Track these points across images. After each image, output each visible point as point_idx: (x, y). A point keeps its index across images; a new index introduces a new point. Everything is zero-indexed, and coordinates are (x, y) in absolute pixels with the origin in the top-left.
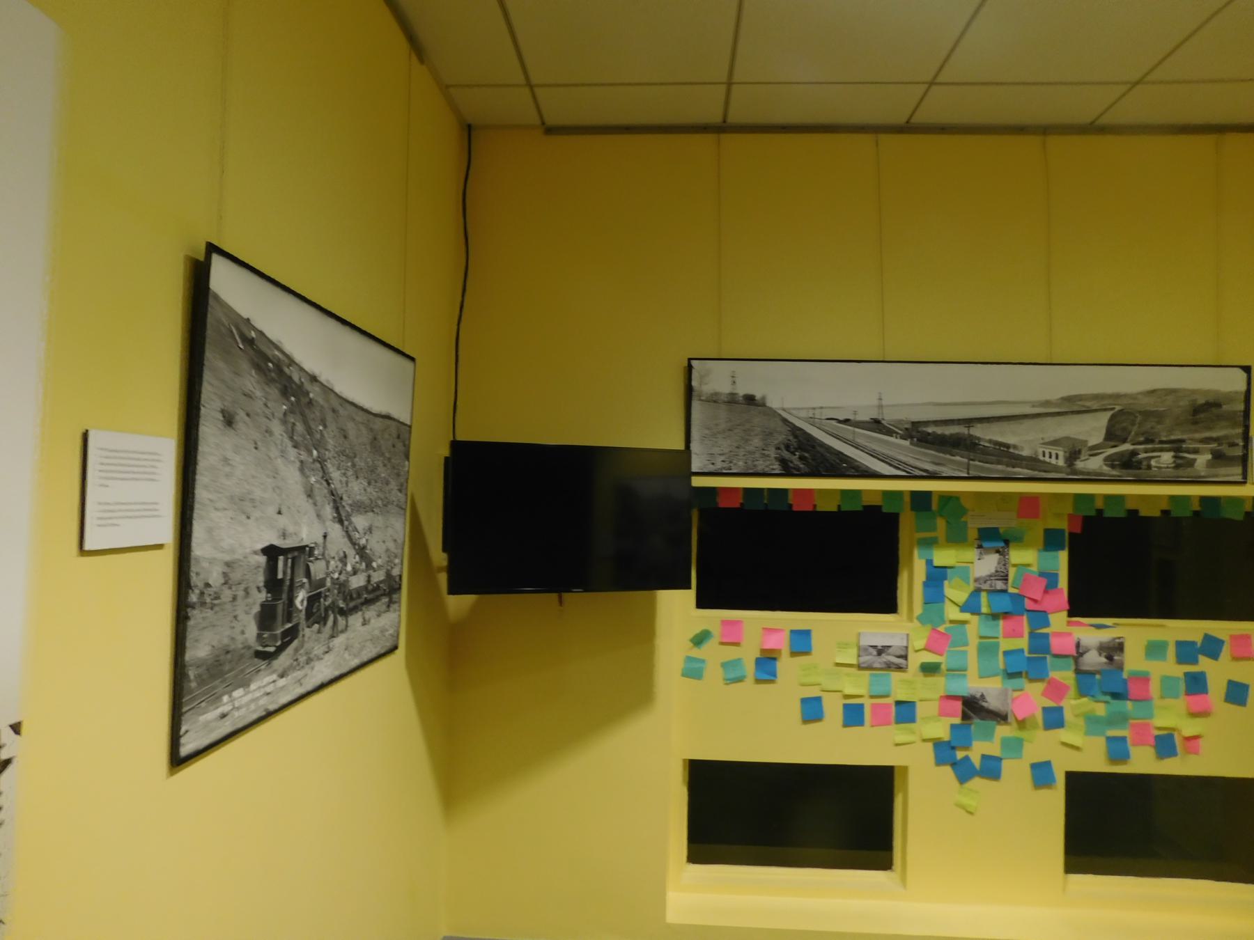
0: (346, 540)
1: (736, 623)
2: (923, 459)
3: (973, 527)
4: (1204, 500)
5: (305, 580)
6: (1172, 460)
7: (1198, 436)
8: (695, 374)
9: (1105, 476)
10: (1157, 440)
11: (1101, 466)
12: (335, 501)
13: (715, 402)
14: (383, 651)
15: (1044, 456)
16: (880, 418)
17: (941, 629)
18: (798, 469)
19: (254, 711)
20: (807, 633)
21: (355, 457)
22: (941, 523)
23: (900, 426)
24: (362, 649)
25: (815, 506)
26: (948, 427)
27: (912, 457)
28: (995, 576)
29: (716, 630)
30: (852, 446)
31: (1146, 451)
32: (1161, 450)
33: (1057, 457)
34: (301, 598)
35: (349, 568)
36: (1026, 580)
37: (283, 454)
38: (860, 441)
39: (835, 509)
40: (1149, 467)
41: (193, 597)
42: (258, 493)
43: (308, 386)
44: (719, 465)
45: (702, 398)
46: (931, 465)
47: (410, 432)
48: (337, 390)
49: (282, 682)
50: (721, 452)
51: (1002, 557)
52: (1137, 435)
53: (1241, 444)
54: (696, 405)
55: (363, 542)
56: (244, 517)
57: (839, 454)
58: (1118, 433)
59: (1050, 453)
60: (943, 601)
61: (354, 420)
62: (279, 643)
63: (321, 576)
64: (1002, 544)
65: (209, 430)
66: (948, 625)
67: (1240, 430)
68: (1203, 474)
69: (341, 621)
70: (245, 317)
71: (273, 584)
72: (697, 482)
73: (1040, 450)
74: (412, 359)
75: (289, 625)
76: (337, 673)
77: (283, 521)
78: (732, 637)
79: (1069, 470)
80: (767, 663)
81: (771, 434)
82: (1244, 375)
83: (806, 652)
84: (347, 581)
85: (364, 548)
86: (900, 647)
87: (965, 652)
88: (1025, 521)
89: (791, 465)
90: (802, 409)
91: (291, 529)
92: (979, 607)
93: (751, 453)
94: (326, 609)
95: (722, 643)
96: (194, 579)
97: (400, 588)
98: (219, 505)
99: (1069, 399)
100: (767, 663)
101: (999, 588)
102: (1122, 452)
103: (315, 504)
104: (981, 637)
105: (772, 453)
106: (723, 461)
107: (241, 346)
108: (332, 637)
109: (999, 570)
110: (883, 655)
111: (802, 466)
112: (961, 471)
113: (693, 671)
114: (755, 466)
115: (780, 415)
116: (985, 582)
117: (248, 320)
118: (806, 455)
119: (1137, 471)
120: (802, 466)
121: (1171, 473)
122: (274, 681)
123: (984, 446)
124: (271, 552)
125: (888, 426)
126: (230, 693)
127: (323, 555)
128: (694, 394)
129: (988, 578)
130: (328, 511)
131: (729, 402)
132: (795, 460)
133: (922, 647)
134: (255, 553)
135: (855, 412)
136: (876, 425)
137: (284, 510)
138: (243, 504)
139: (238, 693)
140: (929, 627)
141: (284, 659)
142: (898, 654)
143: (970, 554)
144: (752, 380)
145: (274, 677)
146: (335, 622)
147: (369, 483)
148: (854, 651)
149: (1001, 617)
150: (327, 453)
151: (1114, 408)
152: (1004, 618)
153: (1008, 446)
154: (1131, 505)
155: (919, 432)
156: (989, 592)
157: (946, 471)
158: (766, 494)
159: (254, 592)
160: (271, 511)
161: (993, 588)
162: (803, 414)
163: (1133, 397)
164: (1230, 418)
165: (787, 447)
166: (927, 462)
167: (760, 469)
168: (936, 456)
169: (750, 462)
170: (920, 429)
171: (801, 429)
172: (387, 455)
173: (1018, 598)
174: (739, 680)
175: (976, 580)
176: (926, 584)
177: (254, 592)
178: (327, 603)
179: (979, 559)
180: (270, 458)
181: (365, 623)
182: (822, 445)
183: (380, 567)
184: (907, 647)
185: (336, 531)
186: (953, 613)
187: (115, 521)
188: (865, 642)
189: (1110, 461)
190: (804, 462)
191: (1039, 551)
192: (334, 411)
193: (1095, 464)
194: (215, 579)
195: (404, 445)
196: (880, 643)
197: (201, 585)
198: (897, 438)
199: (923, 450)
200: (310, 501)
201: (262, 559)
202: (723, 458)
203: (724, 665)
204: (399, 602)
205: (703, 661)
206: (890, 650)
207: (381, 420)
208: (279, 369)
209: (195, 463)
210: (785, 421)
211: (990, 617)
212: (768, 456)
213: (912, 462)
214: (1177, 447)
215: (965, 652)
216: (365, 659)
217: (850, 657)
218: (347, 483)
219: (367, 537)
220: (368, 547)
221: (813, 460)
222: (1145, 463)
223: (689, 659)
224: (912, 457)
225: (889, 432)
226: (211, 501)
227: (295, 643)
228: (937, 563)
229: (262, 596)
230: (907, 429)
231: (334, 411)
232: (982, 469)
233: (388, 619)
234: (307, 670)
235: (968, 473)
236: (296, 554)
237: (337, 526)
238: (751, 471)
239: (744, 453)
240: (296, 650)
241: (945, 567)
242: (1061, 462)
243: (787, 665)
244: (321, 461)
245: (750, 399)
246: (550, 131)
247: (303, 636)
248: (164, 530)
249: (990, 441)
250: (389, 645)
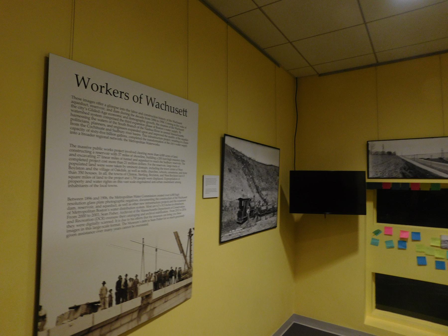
0: (260, 197)
1: (391, 228)
5: (249, 207)
8: (369, 146)
12: (257, 188)
14: (272, 227)
18: (409, 176)
19: (237, 235)
20: (418, 234)
21: (262, 177)
24: (265, 226)
25: (420, 188)
29: (383, 230)
34: (248, 211)
35: (261, 204)
37: (243, 177)
38: (433, 165)
41: (223, 209)
42: (237, 186)
43: (248, 161)
44: (379, 175)
47: (279, 168)
48: (256, 160)
49: (243, 230)
54: (370, 157)
55: (265, 198)
56: (234, 192)
61: (261, 167)
62: (243, 221)
63: (253, 206)
65: (226, 174)
69: (259, 218)
70: (179, 236)
71: (241, 207)
72: (368, 181)
74: (279, 149)
75: (245, 217)
76: (258, 230)
77: (243, 193)
78: (389, 233)
80: (403, 243)
81: (397, 164)
83: (418, 240)
84: (260, 208)
85: (265, 199)
90: (410, 155)
91: (245, 194)
93: (390, 171)
94: (255, 214)
95: (386, 235)
96: (223, 205)
97: (277, 211)
98: (229, 189)
100: (403, 243)
103: (251, 188)
105: (398, 170)
107: (232, 154)
108: (257, 221)
111: (410, 175)
113: (375, 243)
115: (401, 158)
117: (233, 148)
122: (242, 230)
124: (240, 200)
126: (231, 230)
127: (254, 201)
130: (255, 190)
132: (407, 173)
134: (237, 200)
135: (431, 156)
137: (243, 190)
138: (233, 189)
139: (233, 231)
141: (244, 225)
144: (389, 147)
145: (241, 229)
146: (257, 218)
147: (266, 183)
148: (439, 242)
150: (254, 176)
159: (237, 208)
160: (240, 190)
162: (410, 157)
165: (405, 169)
167: (394, 176)
172: (272, 175)
174: (392, 247)
177: (237, 208)
178: (255, 213)
180: (240, 178)
181: (266, 219)
183: (270, 205)
185: (257, 195)
187: (209, 192)
192: (256, 166)
194: (228, 205)
195: (277, 172)
197: (225, 206)
200: (250, 188)
201: (238, 201)
203: (386, 242)
204: (277, 214)
205: (378, 240)
207: (269, 166)
208: (241, 157)
209: (223, 181)
210: (403, 160)
216: (267, 228)
217: (438, 243)
218: (260, 183)
219: (266, 197)
220: (266, 199)
223: (373, 239)
226: (227, 188)
227: (247, 222)
229: (238, 210)
231: (256, 166)
233: (273, 219)
234: (250, 228)
236: (246, 200)
237: (257, 194)
238: (390, 177)
239: (388, 171)
240: (247, 223)
243: (410, 244)
244: (253, 178)
245: (390, 153)
246: (320, 75)
247: (249, 220)
248: (217, 194)
250: (274, 226)
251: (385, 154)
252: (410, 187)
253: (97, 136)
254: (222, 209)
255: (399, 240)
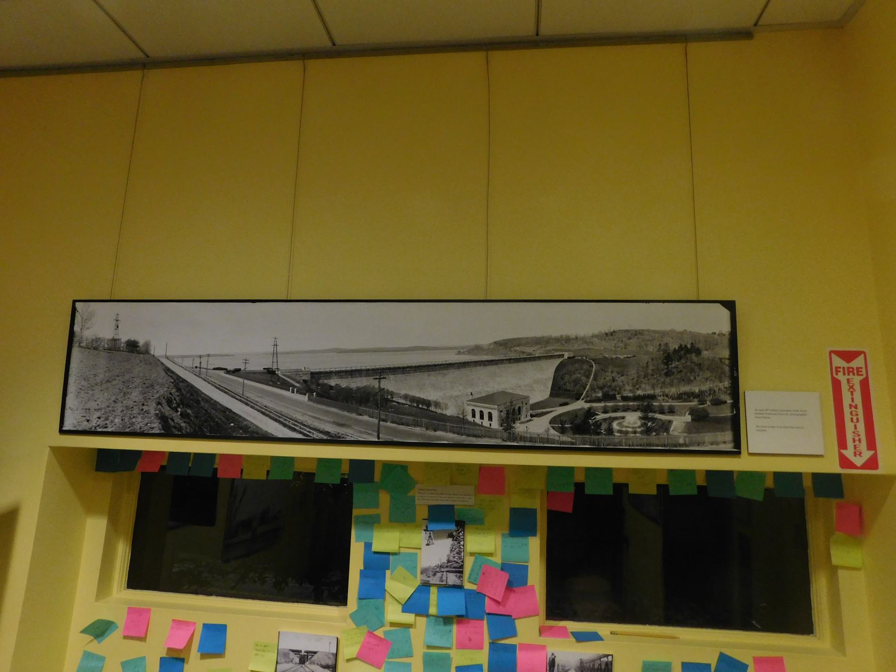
2: (322, 417)
3: (422, 504)
4: (711, 474)
6: (639, 423)
7: (673, 391)
9: (554, 444)
10: (618, 397)
11: (547, 431)
13: (95, 349)
15: (474, 416)
16: (275, 367)
17: (380, 633)
20: (221, 630)
22: (384, 499)
23: (298, 378)
26: (354, 380)
27: (309, 416)
28: (447, 567)
30: (240, 401)
31: (605, 411)
32: (626, 409)
33: (490, 417)
36: (485, 572)
38: (252, 396)
39: (263, 477)
40: (610, 431)
45: (83, 344)
46: (334, 426)
50: (97, 407)
51: (456, 543)
52: (593, 389)
53: (729, 401)
57: (226, 411)
58: (569, 387)
59: (481, 412)
60: (384, 598)
64: (452, 527)
66: (387, 628)
67: (727, 383)
68: (681, 441)
73: (469, 409)
79: (505, 435)
82: (725, 313)
86: (327, 655)
87: (409, 665)
88: (487, 497)
89: (172, 424)
92: (427, 607)
99: (505, 344)
101: (450, 583)
102: (575, 411)
104: (429, 647)
105: (152, 408)
106: (99, 418)
109: (451, 558)
110: (307, 663)
111: (183, 425)
112: (369, 434)
114: (133, 424)
116: (434, 575)
118: (189, 411)
119: (596, 437)
120: (183, 425)
121: (639, 439)
123: (398, 403)
125: (282, 376)
128: (76, 339)
129: (438, 570)
131: (110, 349)
133: (355, 656)
136: (270, 376)
140: (364, 630)
142: (323, 663)
143: (418, 538)
149: (455, 620)
151: (563, 355)
152: (459, 622)
153: (428, 403)
154: (618, 479)
155: (318, 385)
156: (440, 587)
157: (351, 434)
158: (192, 457)
161: (444, 583)
162: (188, 363)
163: (584, 340)
164: (714, 367)
165: (169, 402)
166: (329, 422)
167: (137, 428)
168: (338, 414)
169: (126, 419)
170: (321, 381)
171: (184, 381)
173: (477, 596)
175: (424, 571)
176: (363, 574)
179: (428, 545)
182: (208, 400)
184: (336, 655)
186: (393, 613)
188: (288, 644)
189: (559, 423)
190: (187, 420)
191: (503, 535)
193: (540, 426)
196: (304, 647)
198: (293, 392)
199: (324, 407)
202: (98, 414)
205: (102, 659)
206: (315, 657)
210: (168, 370)
211: (441, 619)
212: (147, 412)
213: (317, 424)
214: (645, 405)
215: (409, 665)
221: (196, 417)
222: (604, 426)
224: (309, 416)
225: (285, 385)
228: (376, 547)
230: (305, 381)
232: (396, 432)
235: (379, 438)
238: (127, 430)
241: (388, 554)
242: (495, 425)
245: (132, 346)
249: (406, 397)
251: (119, 350)
252: (215, 466)
253: (790, 411)
254: (291, 479)
255: (164, 654)
